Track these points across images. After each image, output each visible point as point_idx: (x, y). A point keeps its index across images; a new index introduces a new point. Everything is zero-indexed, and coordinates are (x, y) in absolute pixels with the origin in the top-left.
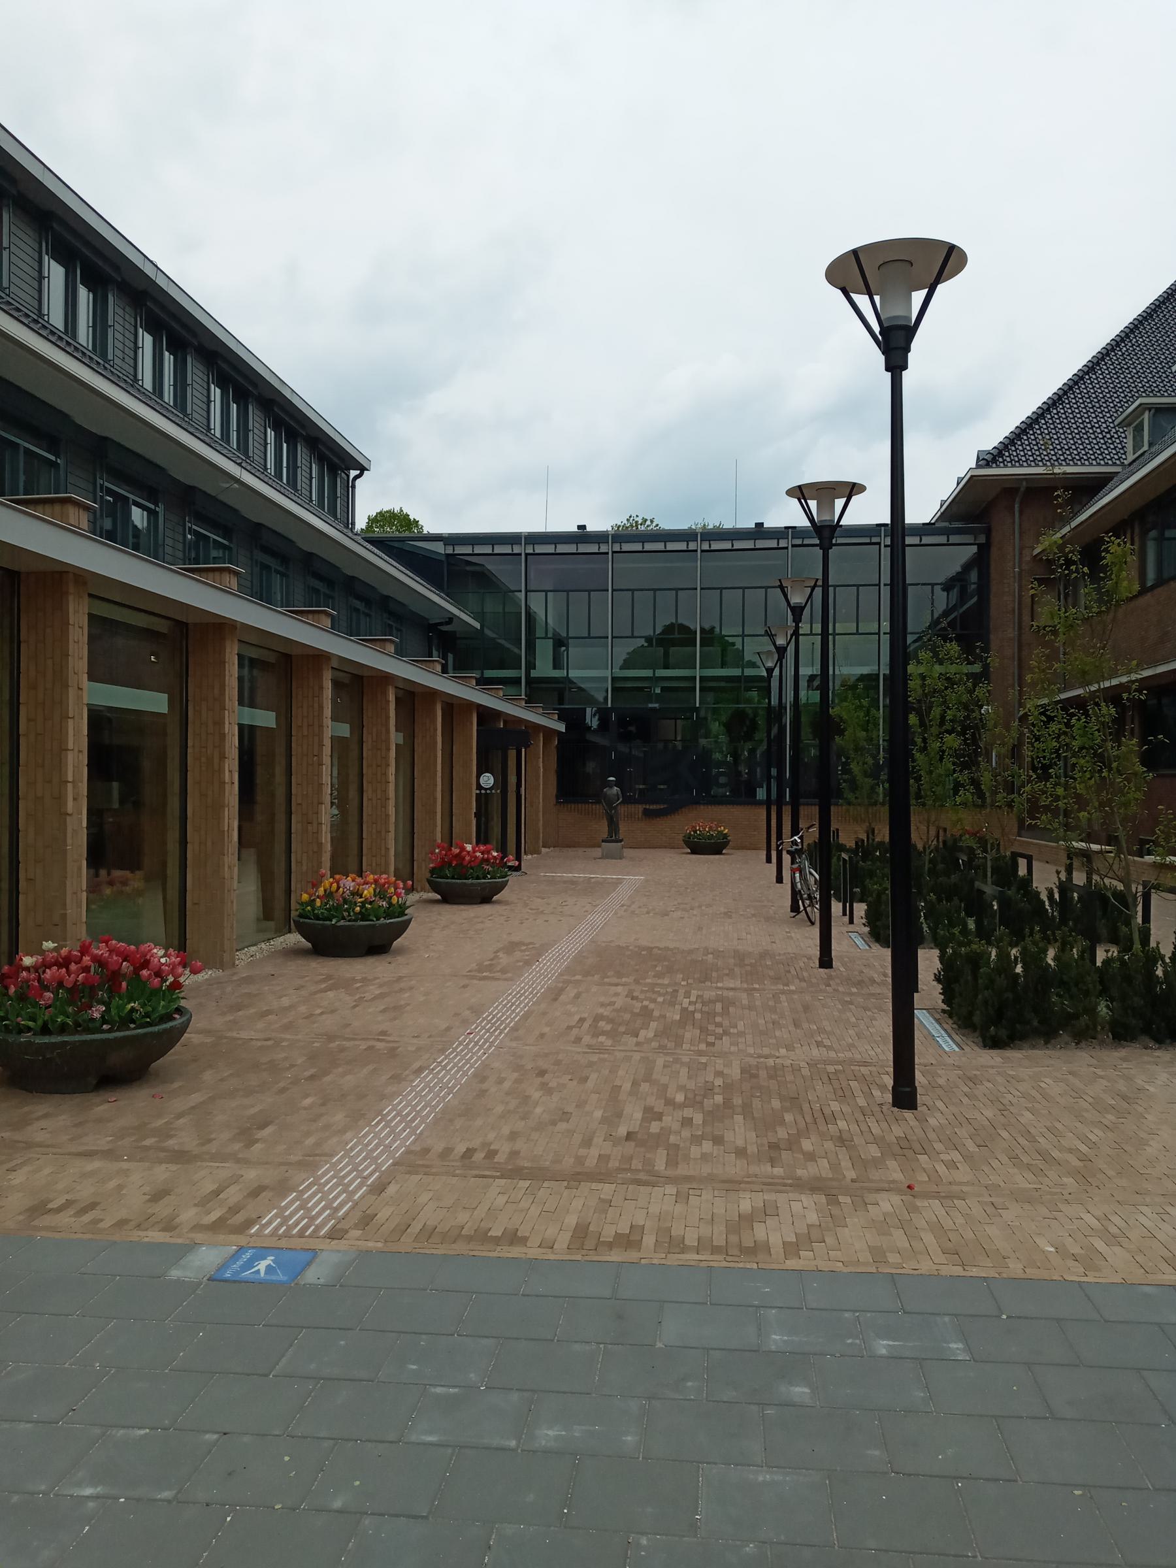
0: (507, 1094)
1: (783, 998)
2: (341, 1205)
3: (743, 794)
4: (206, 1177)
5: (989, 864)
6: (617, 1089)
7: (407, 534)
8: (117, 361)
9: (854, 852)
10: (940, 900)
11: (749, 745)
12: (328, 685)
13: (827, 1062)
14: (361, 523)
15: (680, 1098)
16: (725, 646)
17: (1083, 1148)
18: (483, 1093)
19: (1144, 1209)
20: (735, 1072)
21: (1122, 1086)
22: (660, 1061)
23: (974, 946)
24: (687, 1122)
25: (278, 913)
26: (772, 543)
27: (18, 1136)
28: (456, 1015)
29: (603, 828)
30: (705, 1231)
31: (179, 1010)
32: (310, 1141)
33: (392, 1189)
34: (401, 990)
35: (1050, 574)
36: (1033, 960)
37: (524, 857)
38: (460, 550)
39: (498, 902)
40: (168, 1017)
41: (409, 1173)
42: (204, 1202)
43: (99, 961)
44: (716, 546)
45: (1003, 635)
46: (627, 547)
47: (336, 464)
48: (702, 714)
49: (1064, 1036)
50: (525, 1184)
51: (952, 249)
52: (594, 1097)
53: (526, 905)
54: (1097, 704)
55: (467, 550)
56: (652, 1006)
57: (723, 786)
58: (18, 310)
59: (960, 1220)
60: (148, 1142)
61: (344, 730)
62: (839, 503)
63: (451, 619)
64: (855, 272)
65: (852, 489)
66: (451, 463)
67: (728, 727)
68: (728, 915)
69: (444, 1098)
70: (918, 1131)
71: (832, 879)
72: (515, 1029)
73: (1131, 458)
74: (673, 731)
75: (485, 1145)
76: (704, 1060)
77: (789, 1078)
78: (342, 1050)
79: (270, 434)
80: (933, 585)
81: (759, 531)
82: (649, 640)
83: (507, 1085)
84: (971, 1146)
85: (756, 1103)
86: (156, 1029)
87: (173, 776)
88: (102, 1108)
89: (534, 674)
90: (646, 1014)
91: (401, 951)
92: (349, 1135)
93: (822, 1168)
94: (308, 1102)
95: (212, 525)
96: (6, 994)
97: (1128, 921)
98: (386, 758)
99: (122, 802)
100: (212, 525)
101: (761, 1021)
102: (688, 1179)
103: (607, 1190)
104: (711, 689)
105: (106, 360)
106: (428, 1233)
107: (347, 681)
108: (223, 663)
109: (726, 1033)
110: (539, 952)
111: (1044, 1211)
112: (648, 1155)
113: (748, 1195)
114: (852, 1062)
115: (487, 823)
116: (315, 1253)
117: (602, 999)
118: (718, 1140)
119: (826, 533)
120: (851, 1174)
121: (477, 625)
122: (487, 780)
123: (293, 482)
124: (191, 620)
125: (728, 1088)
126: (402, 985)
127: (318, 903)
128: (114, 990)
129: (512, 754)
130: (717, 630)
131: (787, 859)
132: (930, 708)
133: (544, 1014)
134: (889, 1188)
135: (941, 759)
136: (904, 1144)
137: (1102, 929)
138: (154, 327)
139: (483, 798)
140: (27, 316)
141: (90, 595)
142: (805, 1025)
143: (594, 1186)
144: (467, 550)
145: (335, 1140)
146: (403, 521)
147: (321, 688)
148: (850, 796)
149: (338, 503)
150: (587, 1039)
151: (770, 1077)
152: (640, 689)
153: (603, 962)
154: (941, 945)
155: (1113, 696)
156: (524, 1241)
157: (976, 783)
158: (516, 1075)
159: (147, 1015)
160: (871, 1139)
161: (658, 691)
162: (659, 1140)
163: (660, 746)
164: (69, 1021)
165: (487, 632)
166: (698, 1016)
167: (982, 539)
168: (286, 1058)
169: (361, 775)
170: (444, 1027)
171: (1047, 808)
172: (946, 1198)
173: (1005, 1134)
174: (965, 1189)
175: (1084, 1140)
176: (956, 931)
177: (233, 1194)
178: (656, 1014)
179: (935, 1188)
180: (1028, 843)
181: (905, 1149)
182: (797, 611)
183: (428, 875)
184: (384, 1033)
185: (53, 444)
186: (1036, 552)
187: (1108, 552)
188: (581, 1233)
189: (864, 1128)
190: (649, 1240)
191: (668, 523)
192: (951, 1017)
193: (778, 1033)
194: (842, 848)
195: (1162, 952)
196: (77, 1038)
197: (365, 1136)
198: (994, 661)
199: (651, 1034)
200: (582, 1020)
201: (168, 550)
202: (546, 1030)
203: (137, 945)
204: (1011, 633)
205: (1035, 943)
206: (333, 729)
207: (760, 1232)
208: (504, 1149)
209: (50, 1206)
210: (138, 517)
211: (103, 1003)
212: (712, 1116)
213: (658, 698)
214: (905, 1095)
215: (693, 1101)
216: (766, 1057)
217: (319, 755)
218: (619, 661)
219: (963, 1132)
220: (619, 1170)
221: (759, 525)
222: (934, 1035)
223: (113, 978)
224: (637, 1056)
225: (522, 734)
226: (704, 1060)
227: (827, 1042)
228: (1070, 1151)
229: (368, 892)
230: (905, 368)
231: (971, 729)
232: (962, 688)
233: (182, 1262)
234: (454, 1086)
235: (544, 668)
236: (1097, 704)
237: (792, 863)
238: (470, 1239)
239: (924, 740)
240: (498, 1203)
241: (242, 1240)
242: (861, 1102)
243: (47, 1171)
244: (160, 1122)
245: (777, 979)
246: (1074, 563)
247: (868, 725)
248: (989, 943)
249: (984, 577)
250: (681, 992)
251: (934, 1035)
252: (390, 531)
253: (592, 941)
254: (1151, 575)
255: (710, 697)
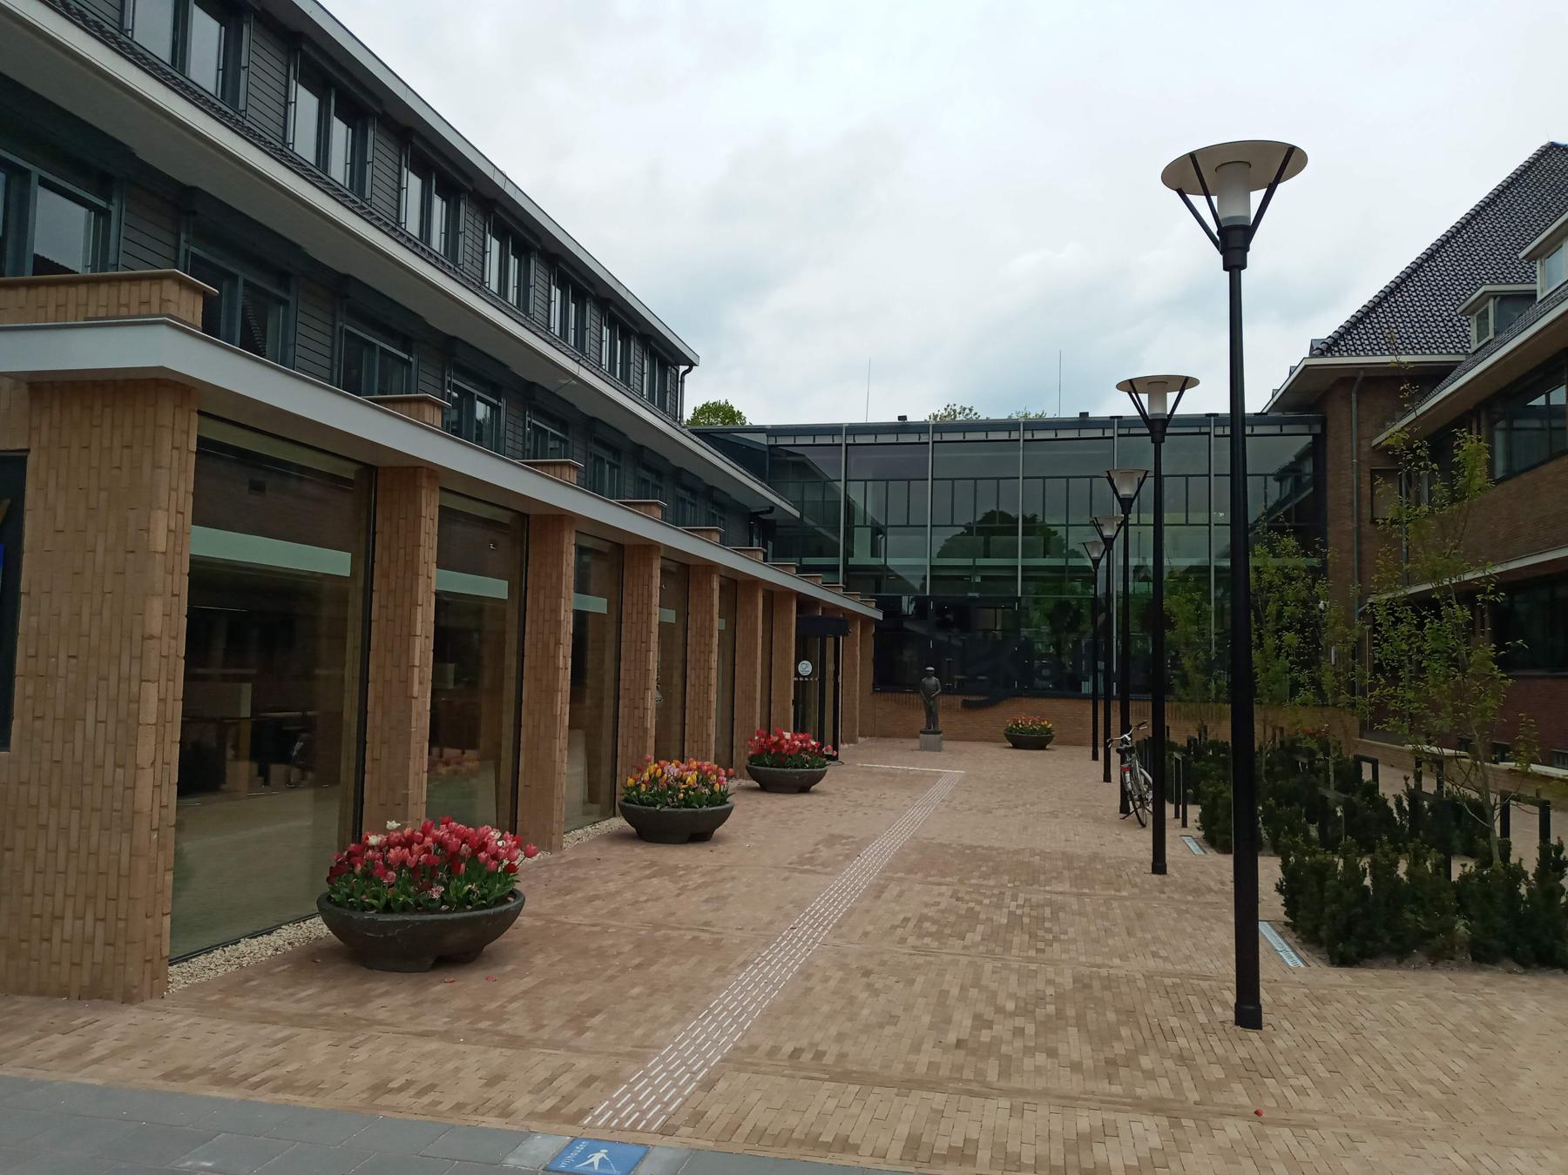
0: (833, 993)
1: (1115, 904)
2: (672, 1100)
3: (1067, 687)
4: (539, 1064)
5: (1331, 768)
6: (944, 994)
7: (730, 426)
8: (467, 265)
9: (1186, 751)
10: (1279, 805)
11: (1073, 636)
12: (657, 573)
13: (1163, 974)
14: (688, 415)
15: (1010, 1006)
16: (1048, 534)
17: (1446, 1080)
18: (808, 990)
19: (1521, 1153)
20: (1067, 981)
21: (1484, 1012)
22: (988, 967)
23: (1320, 857)
24: (1019, 1032)
25: (604, 796)
26: (1098, 433)
27: (359, 1013)
28: (779, 908)
29: (921, 719)
30: (1042, 1148)
31: (513, 894)
32: (639, 1032)
33: (721, 1086)
34: (724, 880)
35: (1388, 465)
36: (1383, 872)
37: (841, 746)
38: (781, 441)
39: (815, 792)
40: (504, 900)
41: (738, 1070)
42: (538, 1090)
43: (440, 843)
44: (1038, 435)
45: (1341, 528)
46: (947, 437)
47: (666, 359)
48: (1023, 603)
49: (1419, 956)
50: (854, 1088)
51: (1291, 150)
52: (922, 1001)
53: (844, 797)
54: (1451, 606)
55: (790, 441)
56: (978, 908)
57: (1044, 678)
58: (379, 219)
59: (1314, 1152)
60: (484, 1025)
61: (671, 616)
62: (1171, 397)
63: (772, 508)
64: (1192, 174)
65: (1185, 383)
66: (782, 358)
67: (1051, 618)
68: (1054, 815)
69: (770, 993)
70: (1264, 1052)
71: (1164, 782)
72: (838, 926)
73: (1475, 346)
74: (992, 621)
75: (813, 1045)
76: (1033, 967)
77: (1124, 989)
78: (668, 939)
79: (606, 332)
80: (1266, 476)
81: (1084, 421)
82: (969, 528)
83: (832, 984)
84: (1321, 1070)
85: (1091, 1016)
86: (491, 911)
87: (511, 661)
88: (439, 988)
89: (851, 561)
90: (972, 916)
91: (721, 840)
92: (676, 1028)
93: (1163, 1088)
94: (636, 991)
95: (551, 420)
96: (352, 872)
97: (1487, 833)
98: (710, 645)
99: (456, 681)
100: (551, 420)
101: (1093, 928)
102: (1021, 1092)
103: (938, 1099)
104: (1032, 579)
105: (457, 265)
106: (758, 1134)
107: (674, 569)
108: (560, 553)
109: (1056, 939)
110: (859, 846)
111: (1406, 1147)
112: (980, 1065)
113: (1086, 1113)
114: (1191, 975)
115: (804, 709)
116: (647, 1148)
117: (926, 899)
118: (1052, 1053)
119: (1157, 427)
120: (1194, 1096)
121: (797, 514)
122: (806, 668)
123: (625, 377)
124: (532, 511)
125: (1060, 997)
126: (725, 874)
127: (643, 788)
128: (452, 872)
129: (830, 641)
130: (1040, 518)
131: (1115, 758)
132: (1267, 602)
133: (868, 911)
134: (1236, 1113)
135: (1278, 656)
136: (1250, 1066)
137: (1457, 843)
138: (501, 233)
139: (801, 686)
140: (386, 224)
141: (442, 489)
142: (1139, 934)
143: (925, 1094)
144: (790, 441)
145: (661, 1033)
146: (725, 412)
147: (651, 577)
148: (1180, 691)
149: (666, 395)
150: (912, 940)
151: (1104, 988)
152: (957, 579)
153: (926, 860)
154: (1277, 850)
155: (1467, 594)
156: (855, 1148)
157: (1316, 683)
158: (841, 974)
159: (484, 897)
160: (1214, 1059)
161: (978, 580)
162: (991, 1048)
163: (980, 635)
164: (410, 900)
165: (806, 520)
166: (1026, 920)
167: (1317, 429)
168: (613, 946)
169: (685, 661)
170: (767, 919)
171: (1395, 713)
172: (1299, 1127)
173: (1358, 1060)
174: (1317, 1118)
175: (1447, 1071)
176: (1299, 839)
177: (566, 1083)
178: (983, 916)
179: (1284, 1115)
180: (1372, 745)
181: (1252, 1072)
182: (1126, 503)
183: (747, 762)
184: (707, 923)
185: (406, 343)
186: (1375, 442)
187: (1459, 447)
188: (913, 1145)
189: (1206, 1047)
190: (984, 1155)
191: (986, 413)
192: (1294, 930)
193: (1110, 942)
194: (1173, 747)
195: (1525, 867)
196: (416, 917)
197: (693, 1029)
198: (1332, 554)
199: (978, 938)
200: (906, 920)
201: (509, 443)
202: (870, 928)
203: (476, 828)
204: (1351, 525)
205: (1386, 855)
206: (660, 615)
207: (1100, 1153)
208: (832, 1050)
209: (391, 1085)
210: (481, 411)
211: (443, 884)
212: (1049, 1026)
213: (978, 587)
214: (1248, 1014)
215: (1025, 1010)
216: (1099, 966)
217: (647, 642)
218: (936, 550)
219: (1313, 1057)
220: (950, 1079)
221: (1084, 415)
222: (1278, 950)
223: (453, 858)
224: (964, 960)
225: (839, 622)
226: (1033, 967)
227: (1163, 953)
228: (1431, 1082)
229: (691, 778)
230: (1244, 267)
231: (1310, 627)
232: (1300, 585)
233: (519, 1150)
234: (780, 982)
235: (862, 557)
236: (1451, 606)
237: (1123, 762)
238: (801, 1143)
239: (1260, 636)
240: (828, 1109)
241: (575, 1130)
242: (1202, 1018)
243: (387, 1050)
244: (493, 1006)
245: (1108, 884)
246: (1423, 458)
247: (1200, 618)
248: (1335, 852)
249: (1320, 467)
250: (1009, 894)
251: (1278, 950)
252: (717, 423)
253: (913, 837)
254: (1500, 465)
255: (1032, 586)
